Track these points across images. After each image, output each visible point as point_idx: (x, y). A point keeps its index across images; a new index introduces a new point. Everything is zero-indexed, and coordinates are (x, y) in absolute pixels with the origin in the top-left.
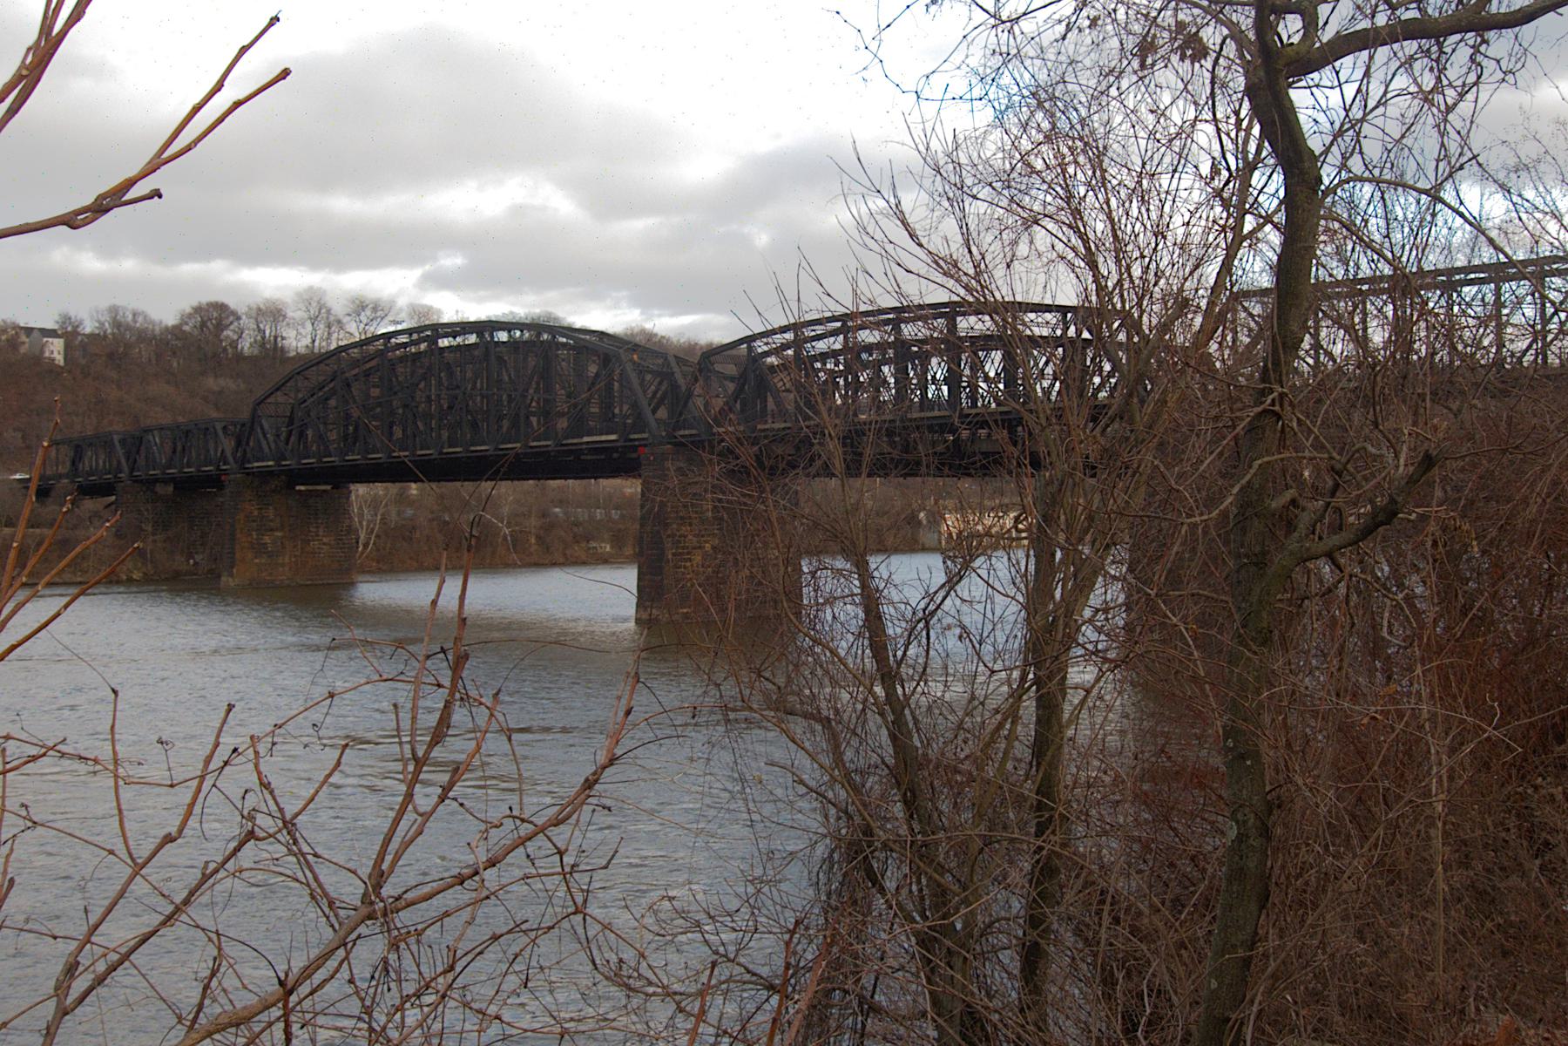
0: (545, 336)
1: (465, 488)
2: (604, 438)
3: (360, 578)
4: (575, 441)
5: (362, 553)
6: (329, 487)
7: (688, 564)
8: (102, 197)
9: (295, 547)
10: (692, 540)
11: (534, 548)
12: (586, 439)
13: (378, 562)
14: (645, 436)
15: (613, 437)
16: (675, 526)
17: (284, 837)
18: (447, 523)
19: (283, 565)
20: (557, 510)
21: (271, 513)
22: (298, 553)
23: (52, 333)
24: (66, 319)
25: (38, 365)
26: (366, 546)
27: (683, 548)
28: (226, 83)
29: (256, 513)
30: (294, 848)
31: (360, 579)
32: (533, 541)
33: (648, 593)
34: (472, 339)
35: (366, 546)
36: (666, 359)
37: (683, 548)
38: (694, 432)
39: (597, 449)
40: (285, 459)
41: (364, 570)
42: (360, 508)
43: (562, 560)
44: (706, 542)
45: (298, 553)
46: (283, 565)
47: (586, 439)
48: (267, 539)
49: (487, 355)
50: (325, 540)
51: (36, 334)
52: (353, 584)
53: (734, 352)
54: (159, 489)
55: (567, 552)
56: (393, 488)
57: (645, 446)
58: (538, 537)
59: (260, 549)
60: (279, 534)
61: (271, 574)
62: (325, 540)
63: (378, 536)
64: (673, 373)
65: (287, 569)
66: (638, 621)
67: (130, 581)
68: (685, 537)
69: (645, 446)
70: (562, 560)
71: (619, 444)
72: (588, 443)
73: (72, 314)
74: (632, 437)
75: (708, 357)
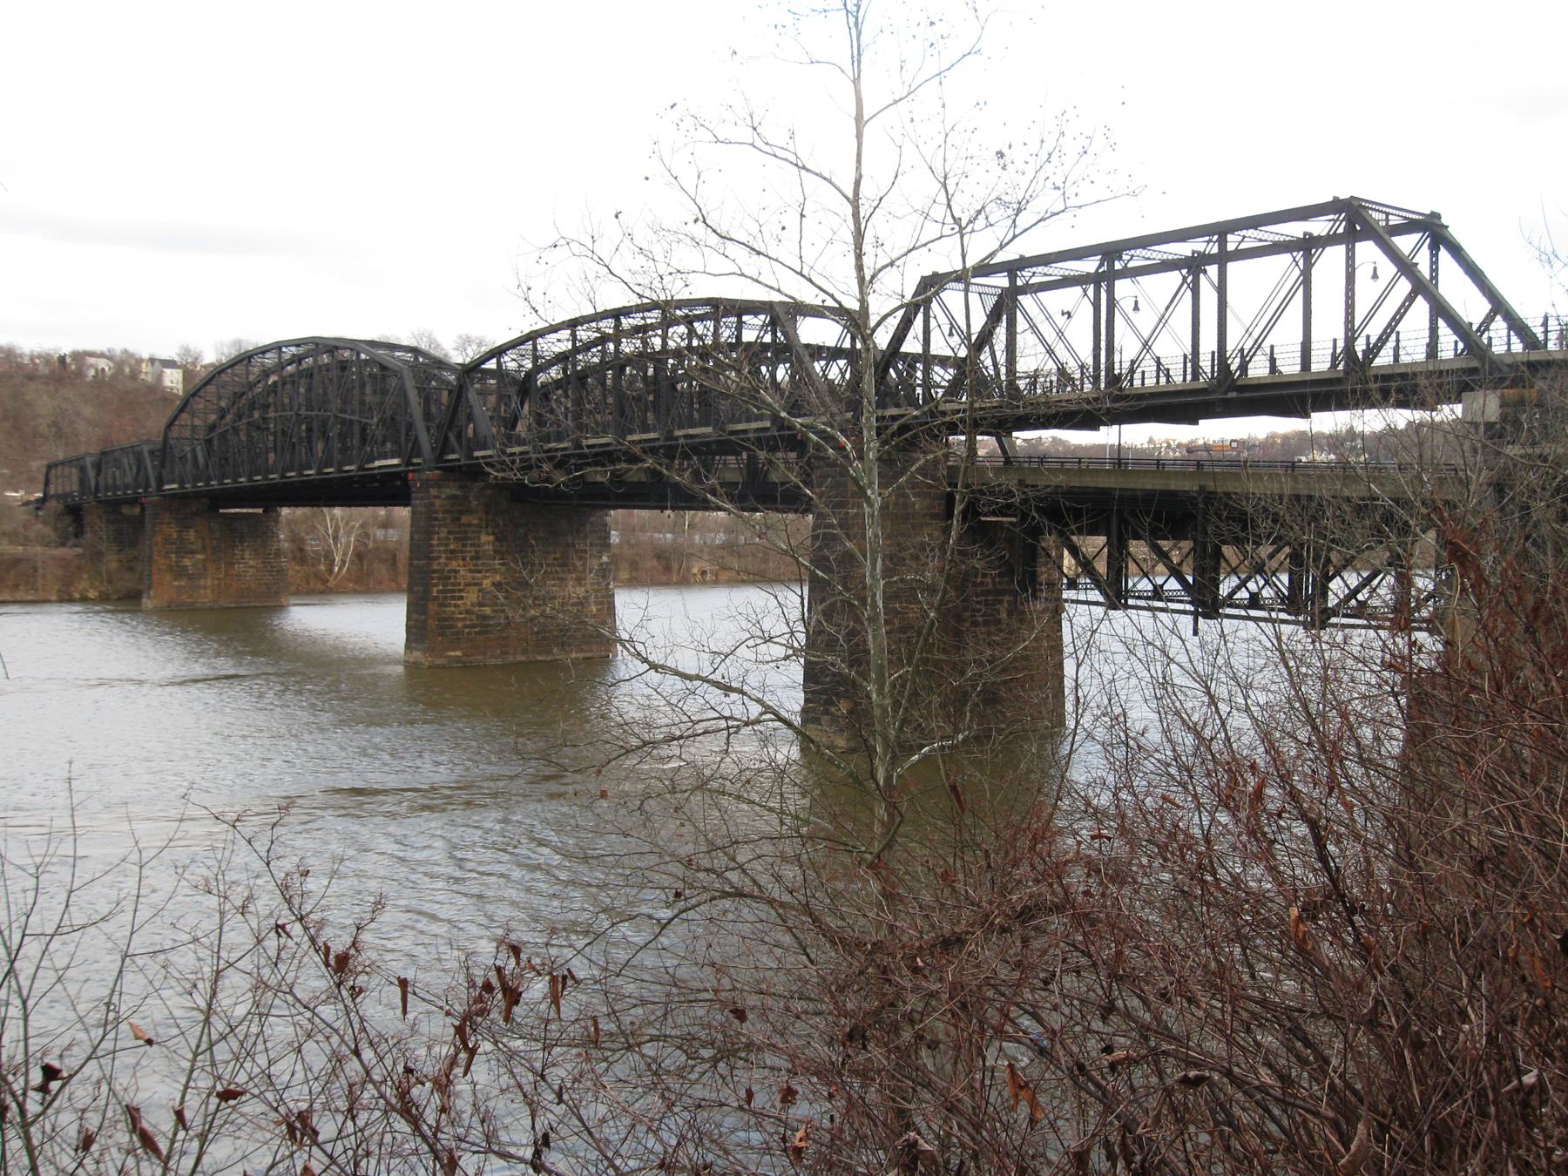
0: (434, 383)
3: (293, 600)
6: (260, 511)
7: (460, 602)
10: (464, 575)
12: (377, 463)
15: (395, 461)
16: (443, 560)
17: (252, 908)
19: (205, 587)
21: (191, 535)
22: (222, 576)
23: (170, 364)
24: (187, 351)
25: (155, 391)
27: (453, 585)
30: (1258, 1097)
31: (292, 602)
33: (416, 631)
37: (453, 585)
41: (298, 593)
44: (485, 577)
45: (222, 576)
46: (205, 587)
47: (377, 463)
48: (187, 562)
50: (251, 563)
51: (157, 365)
52: (281, 608)
54: (126, 510)
59: (180, 572)
60: (200, 556)
61: (191, 597)
62: (251, 563)
65: (209, 591)
67: (84, 600)
68: (456, 572)
72: (380, 467)
73: (192, 347)
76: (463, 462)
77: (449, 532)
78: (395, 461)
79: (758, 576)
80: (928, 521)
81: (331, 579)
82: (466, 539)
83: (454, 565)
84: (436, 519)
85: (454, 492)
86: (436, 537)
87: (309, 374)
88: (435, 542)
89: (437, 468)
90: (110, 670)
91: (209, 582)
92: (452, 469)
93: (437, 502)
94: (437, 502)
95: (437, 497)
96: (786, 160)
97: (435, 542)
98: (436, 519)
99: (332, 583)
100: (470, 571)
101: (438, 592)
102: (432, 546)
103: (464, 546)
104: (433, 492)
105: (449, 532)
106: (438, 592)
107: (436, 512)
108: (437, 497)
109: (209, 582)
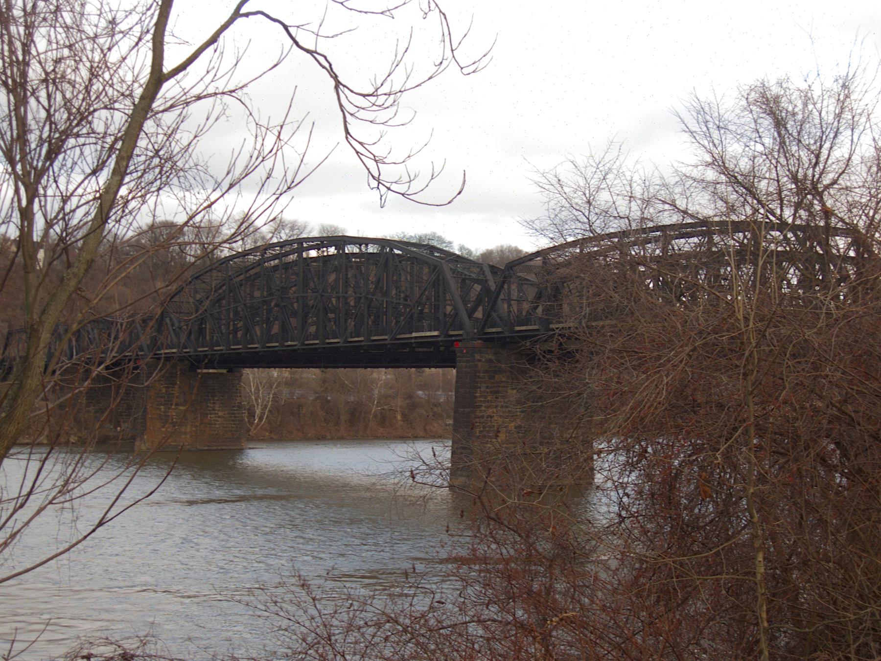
1: (346, 374)
2: (428, 334)
4: (407, 336)
5: (258, 425)
6: (224, 371)
8: (332, 76)
9: (195, 418)
11: (401, 423)
12: (414, 335)
13: (271, 432)
14: (460, 332)
15: (436, 333)
16: (483, 408)
18: (328, 401)
19: (185, 433)
20: (420, 392)
26: (261, 418)
28: (250, 17)
29: (164, 391)
32: (399, 417)
33: (458, 466)
34: (332, 250)
35: (261, 418)
36: (481, 269)
38: (500, 330)
39: (426, 343)
40: (186, 348)
41: (251, 439)
42: (257, 389)
43: (422, 434)
46: (185, 433)
47: (414, 335)
49: (817, 229)
50: (220, 414)
52: (241, 450)
53: (532, 263)
55: (428, 428)
56: (286, 373)
57: (460, 341)
58: (404, 415)
62: (220, 414)
63: (270, 411)
64: (487, 281)
65: (188, 436)
66: (451, 487)
67: (67, 443)
68: (492, 417)
69: (460, 341)
70: (422, 434)
71: (439, 339)
72: (416, 338)
74: (451, 333)
75: (511, 268)
76: (507, 334)
77: (487, 387)
78: (436, 333)
79: (429, 436)
80: (265, 403)
81: (252, 428)
82: (498, 392)
83: (490, 411)
84: (479, 377)
85: (490, 357)
86: (478, 390)
87: (287, 266)
88: (478, 395)
89: (480, 339)
90: (199, 495)
91: (188, 429)
92: (491, 340)
93: (480, 364)
94: (480, 364)
95: (480, 361)
96: (352, 91)
97: (478, 395)
98: (479, 377)
99: (253, 432)
100: (500, 416)
101: (480, 432)
102: (476, 397)
103: (497, 398)
104: (477, 357)
105: (487, 387)
106: (480, 432)
107: (479, 372)
108: (480, 361)
109: (188, 429)
